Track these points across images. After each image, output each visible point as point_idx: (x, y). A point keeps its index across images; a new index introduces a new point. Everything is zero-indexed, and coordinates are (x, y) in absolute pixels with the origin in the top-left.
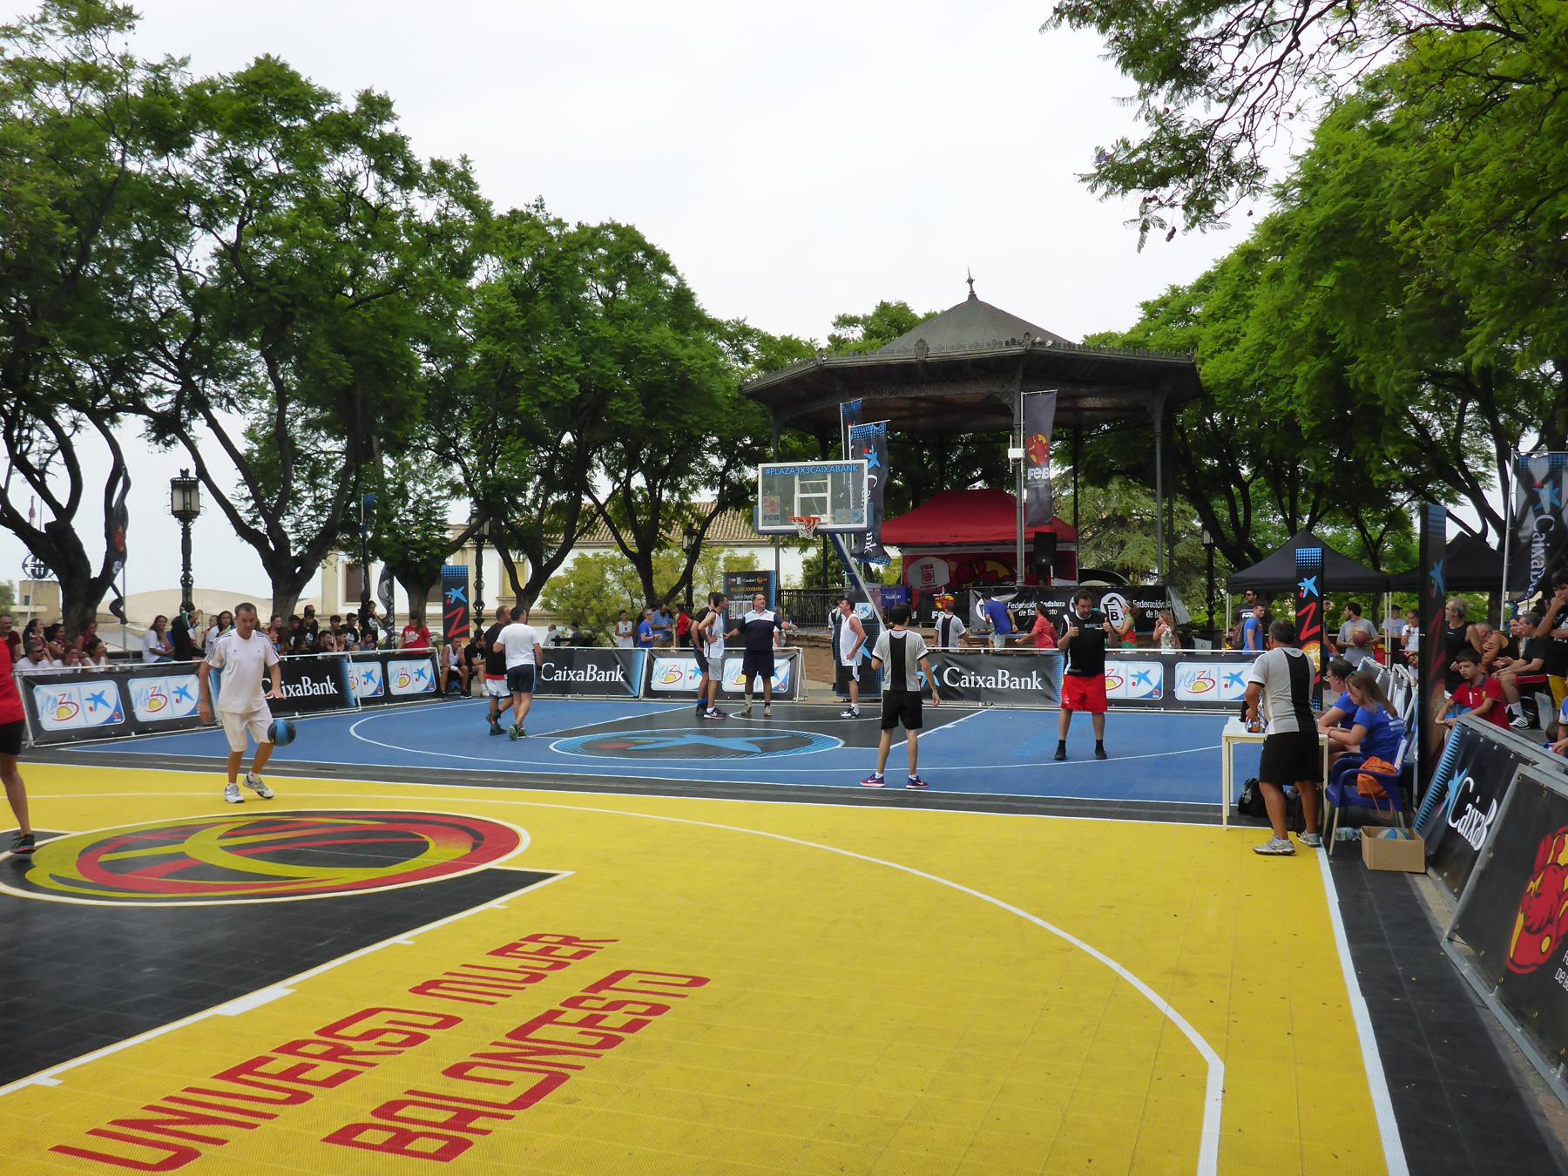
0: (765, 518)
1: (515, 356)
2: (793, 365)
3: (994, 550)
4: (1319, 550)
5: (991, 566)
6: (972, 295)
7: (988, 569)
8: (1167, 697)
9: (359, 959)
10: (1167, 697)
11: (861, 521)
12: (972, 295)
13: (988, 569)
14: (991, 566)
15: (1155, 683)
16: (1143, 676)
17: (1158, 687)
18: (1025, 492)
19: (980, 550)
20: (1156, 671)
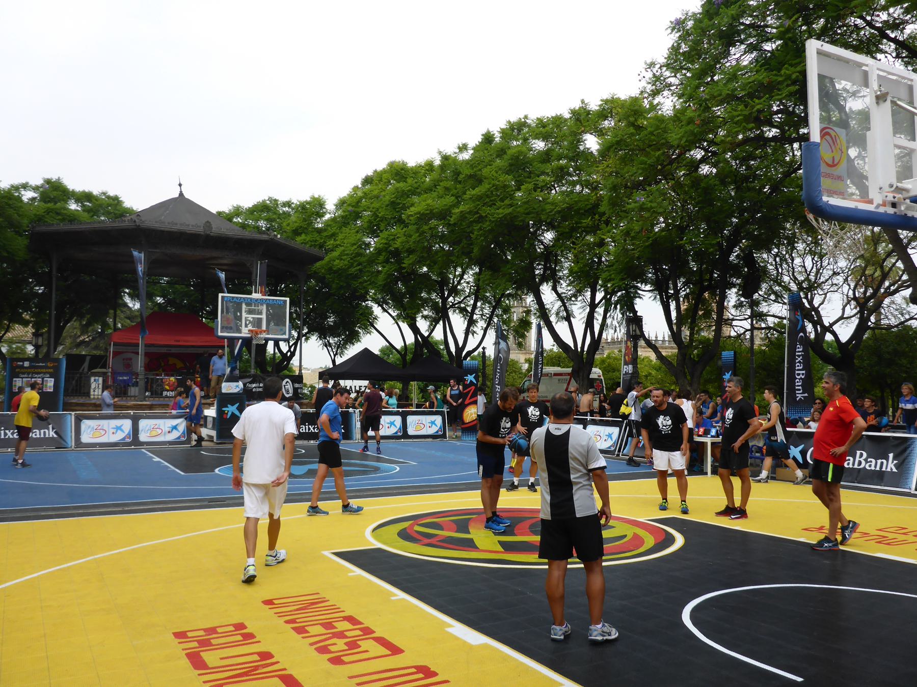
0: (222, 328)
1: (430, 201)
2: (125, 223)
3: (173, 350)
4: (732, 353)
5: (172, 361)
6: (181, 194)
7: (171, 362)
8: (404, 434)
9: (528, 668)
10: (404, 434)
11: (285, 334)
12: (181, 194)
13: (171, 362)
14: (172, 361)
15: (127, 432)
16: (119, 428)
17: (129, 434)
18: (28, 317)
19: (164, 350)
20: (127, 424)
